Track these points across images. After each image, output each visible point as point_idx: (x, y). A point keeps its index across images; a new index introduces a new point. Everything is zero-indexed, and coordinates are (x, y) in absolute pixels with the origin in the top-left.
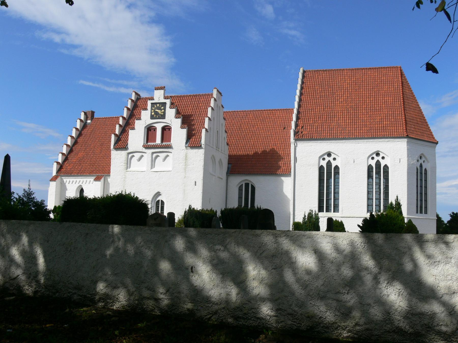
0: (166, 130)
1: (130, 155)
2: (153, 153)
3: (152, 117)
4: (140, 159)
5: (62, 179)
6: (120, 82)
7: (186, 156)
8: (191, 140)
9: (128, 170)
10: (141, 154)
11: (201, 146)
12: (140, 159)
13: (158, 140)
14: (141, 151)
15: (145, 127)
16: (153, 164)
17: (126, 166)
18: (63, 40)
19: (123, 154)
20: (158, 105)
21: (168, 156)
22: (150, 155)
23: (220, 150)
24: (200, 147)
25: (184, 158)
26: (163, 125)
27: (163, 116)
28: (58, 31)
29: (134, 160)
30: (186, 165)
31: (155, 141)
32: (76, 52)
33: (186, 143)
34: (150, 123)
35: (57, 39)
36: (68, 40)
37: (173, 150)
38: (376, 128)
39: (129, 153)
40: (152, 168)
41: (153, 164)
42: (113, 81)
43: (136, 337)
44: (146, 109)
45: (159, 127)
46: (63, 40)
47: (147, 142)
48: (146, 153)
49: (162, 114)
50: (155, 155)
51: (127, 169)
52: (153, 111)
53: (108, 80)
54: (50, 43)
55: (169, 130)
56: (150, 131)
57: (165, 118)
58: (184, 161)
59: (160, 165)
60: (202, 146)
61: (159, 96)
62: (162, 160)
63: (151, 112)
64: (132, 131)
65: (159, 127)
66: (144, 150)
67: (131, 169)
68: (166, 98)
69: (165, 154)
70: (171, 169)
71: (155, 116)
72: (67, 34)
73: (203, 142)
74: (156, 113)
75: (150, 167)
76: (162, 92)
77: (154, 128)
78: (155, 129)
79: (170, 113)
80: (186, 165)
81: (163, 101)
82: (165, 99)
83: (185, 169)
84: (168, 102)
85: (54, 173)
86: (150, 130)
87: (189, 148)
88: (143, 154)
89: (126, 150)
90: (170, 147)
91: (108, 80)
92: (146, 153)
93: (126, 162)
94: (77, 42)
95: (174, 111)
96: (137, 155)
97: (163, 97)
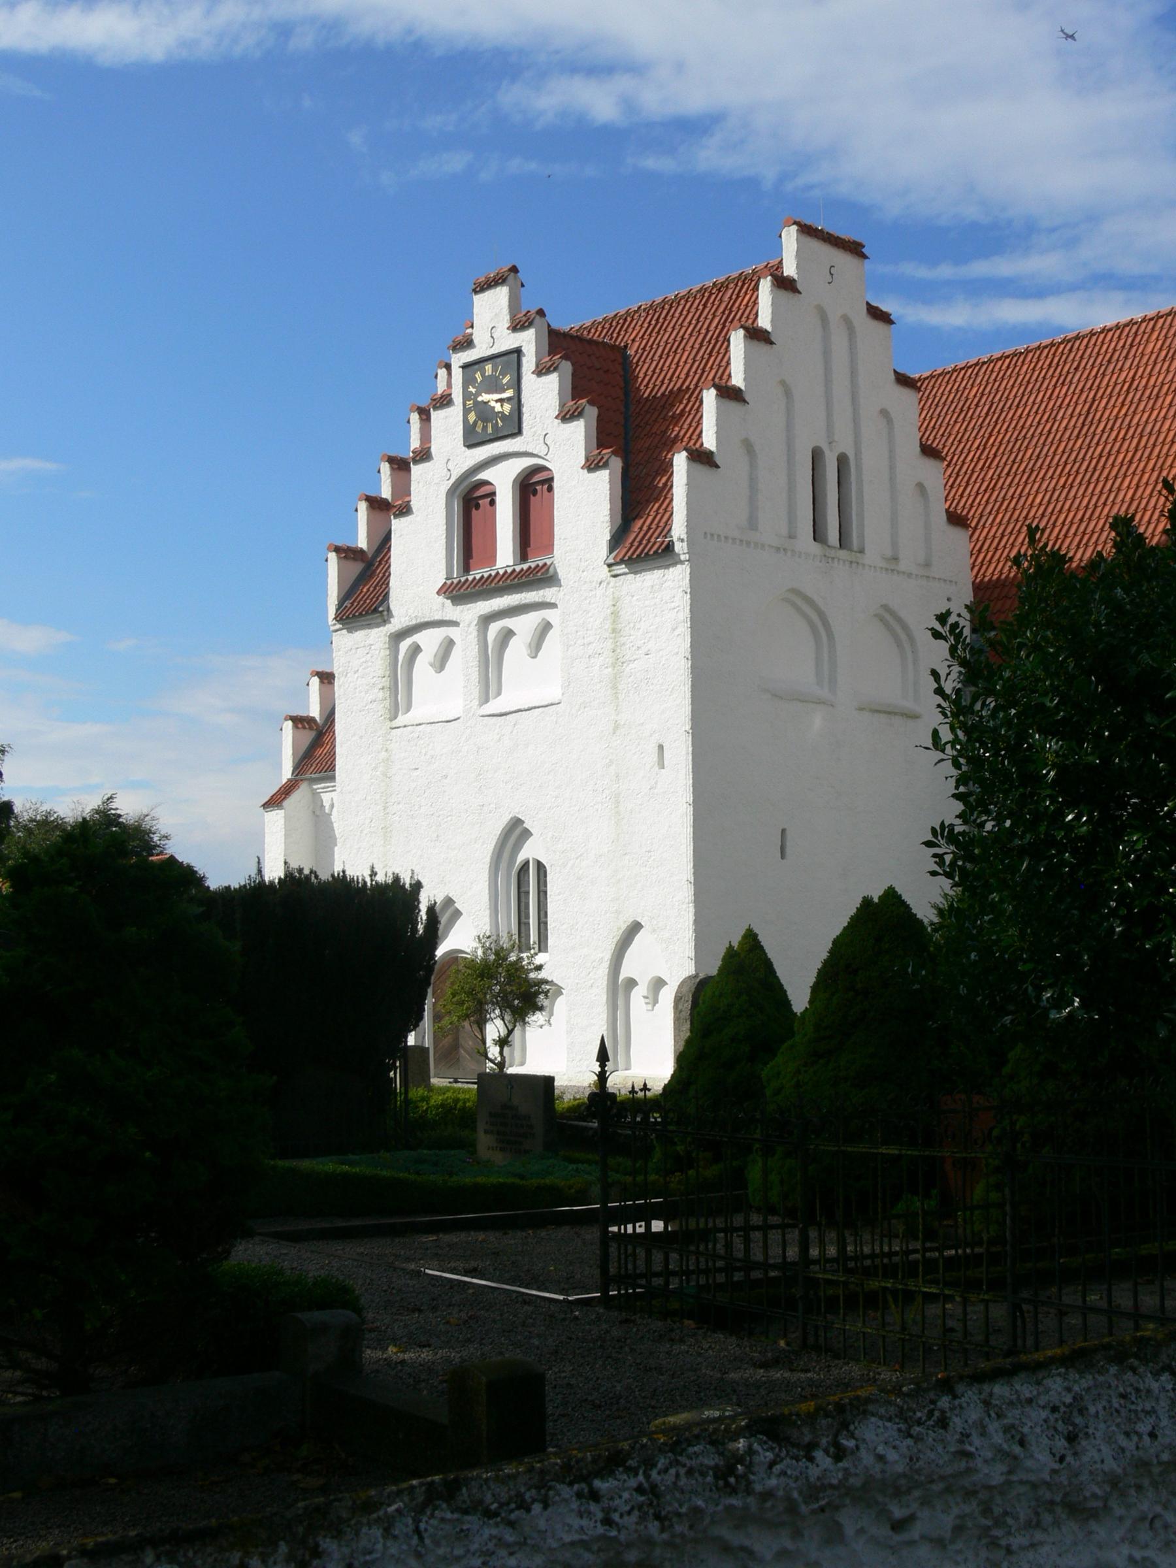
0: (534, 487)
1: (405, 645)
2: (487, 620)
3: (472, 440)
5: (316, 795)
6: (980, 268)
7: (615, 615)
8: (639, 523)
9: (401, 719)
11: (669, 548)
13: (505, 556)
14: (437, 617)
15: (451, 493)
16: (490, 676)
17: (387, 703)
18: (628, 105)
19: (375, 638)
20: (489, 368)
23: (872, 556)
24: (664, 554)
25: (608, 625)
26: (517, 466)
27: (514, 426)
28: (595, 63)
31: (492, 558)
32: (709, 157)
35: (600, 102)
36: (655, 100)
40: (485, 699)
41: (490, 676)
42: (946, 271)
43: (706, 1430)
45: (503, 480)
46: (628, 105)
47: (467, 569)
51: (394, 717)
52: (470, 403)
53: (922, 272)
54: (581, 137)
57: (519, 432)
58: (609, 644)
59: (526, 678)
60: (679, 547)
62: (524, 651)
63: (466, 411)
65: (503, 480)
67: (418, 713)
70: (553, 692)
72: (635, 68)
73: (678, 528)
74: (484, 413)
75: (475, 691)
76: (501, 294)
79: (543, 393)
80: (618, 662)
81: (508, 341)
84: (528, 341)
85: (287, 773)
86: (471, 499)
87: (622, 569)
88: (451, 632)
91: (922, 272)
92: (454, 624)
93: (386, 682)
94: (694, 99)
97: (505, 320)
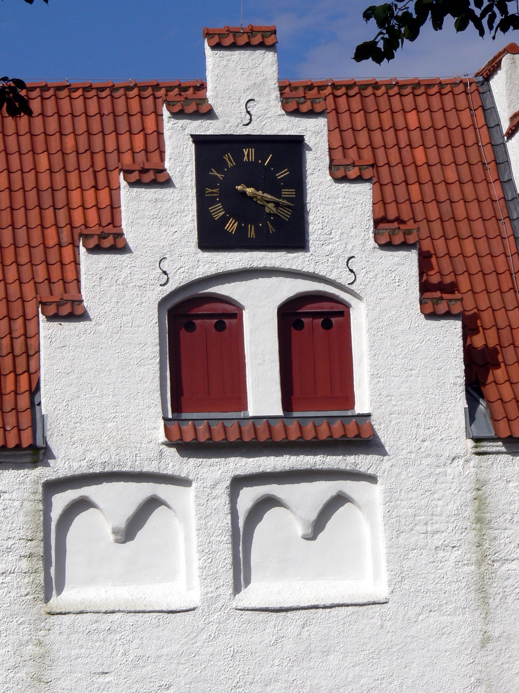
0: (315, 327)
1: (61, 501)
2: (238, 483)
3: (211, 237)
4: (129, 531)
9: (57, 602)
10: (144, 490)
12: (129, 531)
13: (263, 394)
15: (162, 303)
17: (41, 578)
21: (152, 503)
22: (222, 492)
25: (469, 512)
27: (292, 234)
29: (91, 534)
30: (484, 557)
33: (471, 414)
34: (200, 272)
37: (386, 463)
38: (109, 121)
39: (52, 487)
40: (237, 589)
44: (153, 176)
48: (185, 482)
49: (286, 214)
50: (248, 496)
51: (47, 599)
55: (327, 325)
56: (190, 327)
58: (471, 536)
61: (244, 92)
62: (299, 530)
64: (69, 328)
66: (173, 462)
67: (70, 596)
68: (297, 98)
69: (323, 490)
70: (381, 591)
71: (231, 226)
74: (244, 209)
77: (220, 307)
78: (229, 316)
79: (339, 212)
80: (484, 557)
81: (273, 121)
82: (296, 113)
83: (482, 590)
84: (315, 132)
86: (197, 329)
87: (499, 446)
88: (162, 491)
89: (35, 463)
90: (363, 439)
95: (362, 195)
96: (117, 501)
